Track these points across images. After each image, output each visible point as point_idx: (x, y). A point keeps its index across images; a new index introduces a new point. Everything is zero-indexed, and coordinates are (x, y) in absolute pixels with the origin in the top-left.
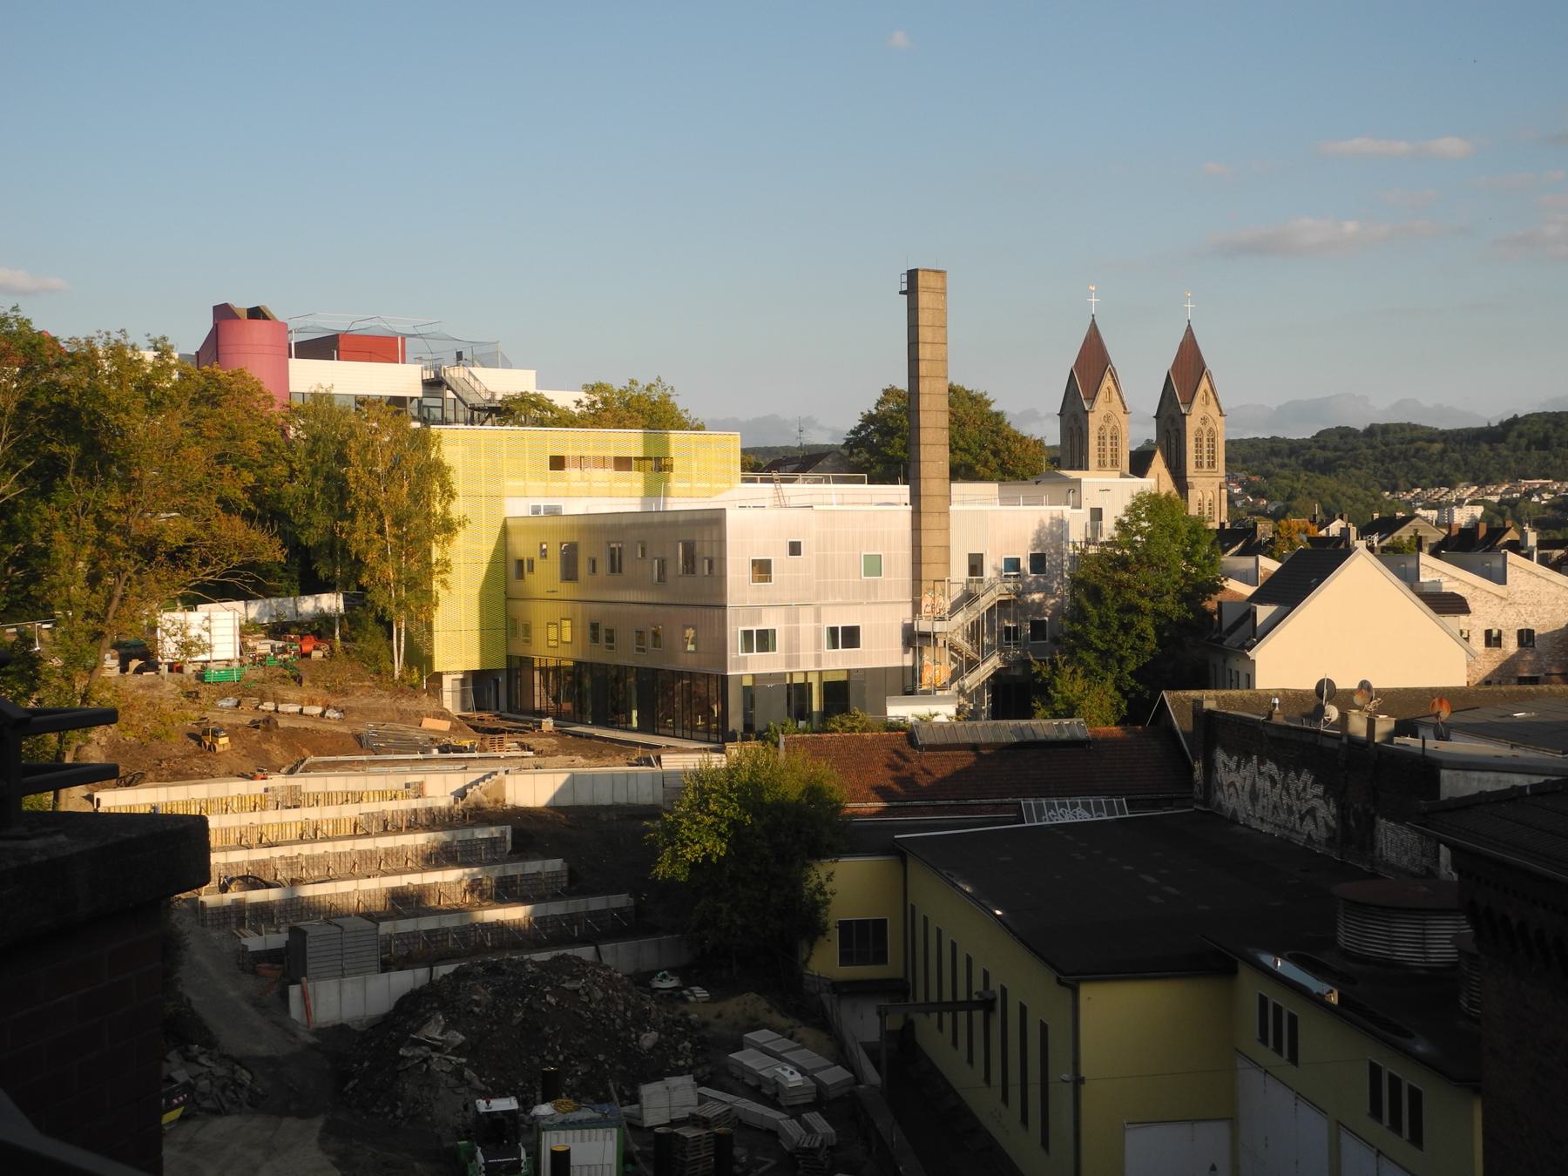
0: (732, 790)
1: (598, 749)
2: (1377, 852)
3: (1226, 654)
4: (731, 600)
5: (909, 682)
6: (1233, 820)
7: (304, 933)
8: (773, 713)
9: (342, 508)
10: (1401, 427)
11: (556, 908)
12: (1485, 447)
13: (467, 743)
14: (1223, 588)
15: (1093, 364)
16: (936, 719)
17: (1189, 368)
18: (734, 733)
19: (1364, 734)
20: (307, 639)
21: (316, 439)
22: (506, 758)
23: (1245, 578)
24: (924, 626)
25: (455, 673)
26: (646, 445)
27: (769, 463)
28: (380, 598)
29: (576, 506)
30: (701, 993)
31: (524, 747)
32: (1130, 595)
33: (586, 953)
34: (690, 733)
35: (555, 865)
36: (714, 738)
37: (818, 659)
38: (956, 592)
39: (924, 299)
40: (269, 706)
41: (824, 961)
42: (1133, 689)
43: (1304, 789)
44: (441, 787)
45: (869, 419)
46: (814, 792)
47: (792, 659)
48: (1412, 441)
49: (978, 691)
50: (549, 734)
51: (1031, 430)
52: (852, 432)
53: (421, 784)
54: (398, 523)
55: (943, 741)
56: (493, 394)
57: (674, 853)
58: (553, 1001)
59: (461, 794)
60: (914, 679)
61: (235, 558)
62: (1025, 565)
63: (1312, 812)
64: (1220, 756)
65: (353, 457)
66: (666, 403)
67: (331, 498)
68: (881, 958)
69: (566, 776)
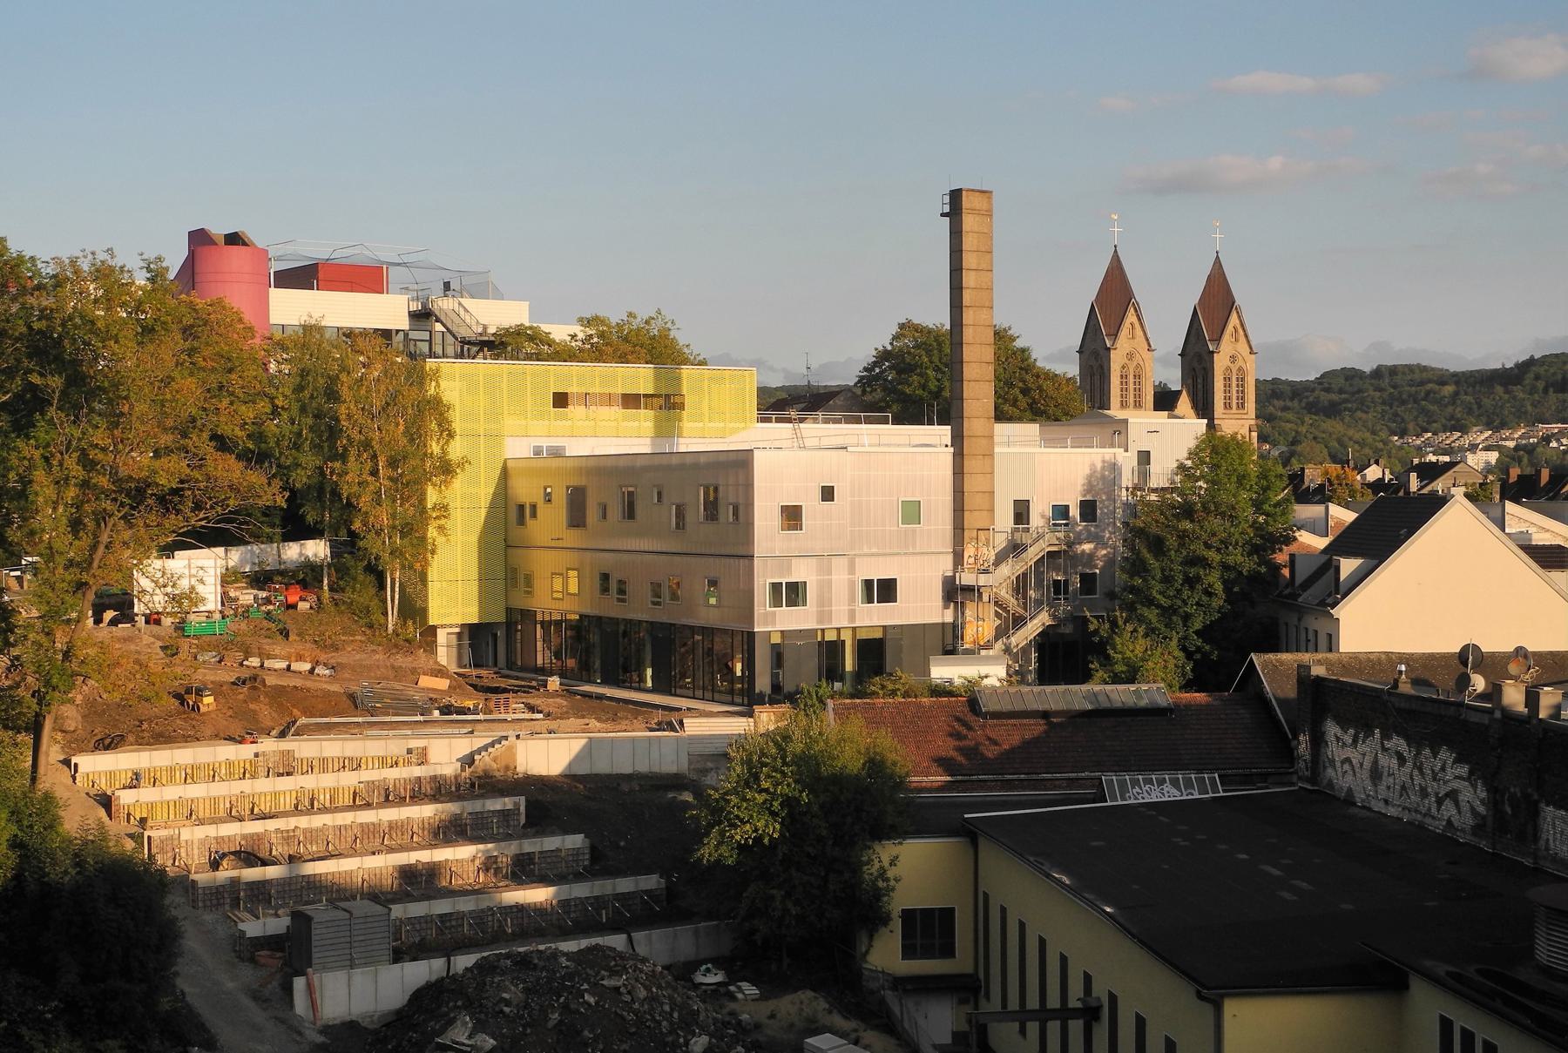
0: (785, 763)
1: (614, 711)
2: (1542, 843)
3: (1301, 611)
4: (759, 550)
5: (949, 640)
6: (1349, 801)
7: (309, 919)
8: (802, 675)
9: (333, 447)
10: (1410, 368)
11: (581, 890)
12: (1499, 389)
13: (470, 704)
14: (1295, 539)
15: (1115, 298)
16: (986, 682)
17: (1217, 302)
18: (761, 695)
19: (1521, 708)
20: (292, 590)
21: (304, 373)
22: (514, 721)
23: (1319, 528)
24: (967, 578)
25: (451, 626)
26: (657, 378)
27: (785, 403)
28: (373, 545)
29: (580, 447)
30: (750, 990)
31: (532, 709)
32: (1198, 548)
33: (617, 941)
34: (710, 693)
35: (575, 841)
36: (738, 700)
37: (852, 615)
38: (1001, 541)
39: (968, 222)
40: (254, 662)
41: (885, 954)
42: (1199, 649)
43: (1443, 769)
44: (446, 753)
45: (884, 356)
46: (875, 765)
47: (823, 615)
48: (1422, 383)
49: (1025, 651)
50: (555, 694)
51: (1058, 368)
52: (866, 369)
53: (425, 749)
54: (393, 463)
55: (1009, 708)
56: (485, 328)
57: (722, 833)
58: (592, 1000)
59: (469, 760)
60: (955, 637)
61: (231, 502)
62: (1075, 512)
63: (1453, 795)
64: (1332, 729)
65: (345, 392)
66: (667, 337)
67: (320, 437)
68: (948, 951)
69: (583, 742)
